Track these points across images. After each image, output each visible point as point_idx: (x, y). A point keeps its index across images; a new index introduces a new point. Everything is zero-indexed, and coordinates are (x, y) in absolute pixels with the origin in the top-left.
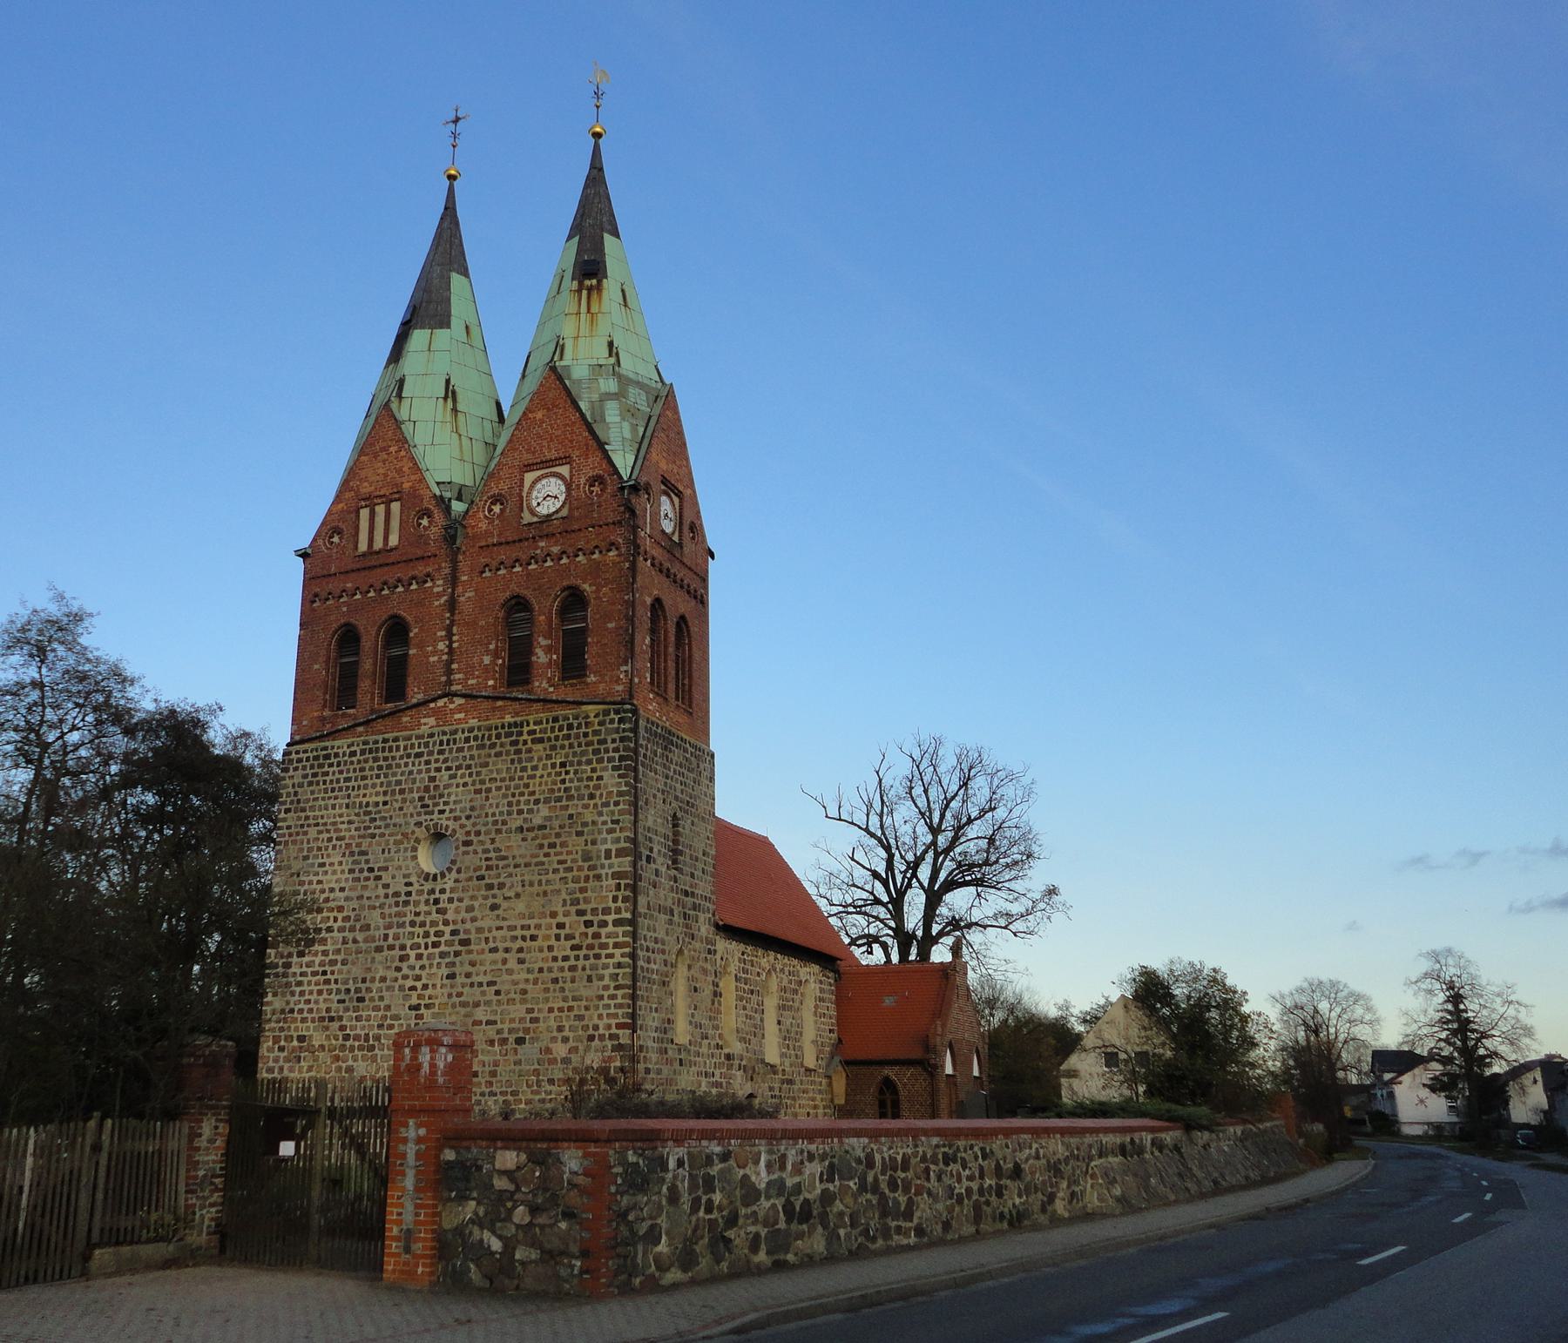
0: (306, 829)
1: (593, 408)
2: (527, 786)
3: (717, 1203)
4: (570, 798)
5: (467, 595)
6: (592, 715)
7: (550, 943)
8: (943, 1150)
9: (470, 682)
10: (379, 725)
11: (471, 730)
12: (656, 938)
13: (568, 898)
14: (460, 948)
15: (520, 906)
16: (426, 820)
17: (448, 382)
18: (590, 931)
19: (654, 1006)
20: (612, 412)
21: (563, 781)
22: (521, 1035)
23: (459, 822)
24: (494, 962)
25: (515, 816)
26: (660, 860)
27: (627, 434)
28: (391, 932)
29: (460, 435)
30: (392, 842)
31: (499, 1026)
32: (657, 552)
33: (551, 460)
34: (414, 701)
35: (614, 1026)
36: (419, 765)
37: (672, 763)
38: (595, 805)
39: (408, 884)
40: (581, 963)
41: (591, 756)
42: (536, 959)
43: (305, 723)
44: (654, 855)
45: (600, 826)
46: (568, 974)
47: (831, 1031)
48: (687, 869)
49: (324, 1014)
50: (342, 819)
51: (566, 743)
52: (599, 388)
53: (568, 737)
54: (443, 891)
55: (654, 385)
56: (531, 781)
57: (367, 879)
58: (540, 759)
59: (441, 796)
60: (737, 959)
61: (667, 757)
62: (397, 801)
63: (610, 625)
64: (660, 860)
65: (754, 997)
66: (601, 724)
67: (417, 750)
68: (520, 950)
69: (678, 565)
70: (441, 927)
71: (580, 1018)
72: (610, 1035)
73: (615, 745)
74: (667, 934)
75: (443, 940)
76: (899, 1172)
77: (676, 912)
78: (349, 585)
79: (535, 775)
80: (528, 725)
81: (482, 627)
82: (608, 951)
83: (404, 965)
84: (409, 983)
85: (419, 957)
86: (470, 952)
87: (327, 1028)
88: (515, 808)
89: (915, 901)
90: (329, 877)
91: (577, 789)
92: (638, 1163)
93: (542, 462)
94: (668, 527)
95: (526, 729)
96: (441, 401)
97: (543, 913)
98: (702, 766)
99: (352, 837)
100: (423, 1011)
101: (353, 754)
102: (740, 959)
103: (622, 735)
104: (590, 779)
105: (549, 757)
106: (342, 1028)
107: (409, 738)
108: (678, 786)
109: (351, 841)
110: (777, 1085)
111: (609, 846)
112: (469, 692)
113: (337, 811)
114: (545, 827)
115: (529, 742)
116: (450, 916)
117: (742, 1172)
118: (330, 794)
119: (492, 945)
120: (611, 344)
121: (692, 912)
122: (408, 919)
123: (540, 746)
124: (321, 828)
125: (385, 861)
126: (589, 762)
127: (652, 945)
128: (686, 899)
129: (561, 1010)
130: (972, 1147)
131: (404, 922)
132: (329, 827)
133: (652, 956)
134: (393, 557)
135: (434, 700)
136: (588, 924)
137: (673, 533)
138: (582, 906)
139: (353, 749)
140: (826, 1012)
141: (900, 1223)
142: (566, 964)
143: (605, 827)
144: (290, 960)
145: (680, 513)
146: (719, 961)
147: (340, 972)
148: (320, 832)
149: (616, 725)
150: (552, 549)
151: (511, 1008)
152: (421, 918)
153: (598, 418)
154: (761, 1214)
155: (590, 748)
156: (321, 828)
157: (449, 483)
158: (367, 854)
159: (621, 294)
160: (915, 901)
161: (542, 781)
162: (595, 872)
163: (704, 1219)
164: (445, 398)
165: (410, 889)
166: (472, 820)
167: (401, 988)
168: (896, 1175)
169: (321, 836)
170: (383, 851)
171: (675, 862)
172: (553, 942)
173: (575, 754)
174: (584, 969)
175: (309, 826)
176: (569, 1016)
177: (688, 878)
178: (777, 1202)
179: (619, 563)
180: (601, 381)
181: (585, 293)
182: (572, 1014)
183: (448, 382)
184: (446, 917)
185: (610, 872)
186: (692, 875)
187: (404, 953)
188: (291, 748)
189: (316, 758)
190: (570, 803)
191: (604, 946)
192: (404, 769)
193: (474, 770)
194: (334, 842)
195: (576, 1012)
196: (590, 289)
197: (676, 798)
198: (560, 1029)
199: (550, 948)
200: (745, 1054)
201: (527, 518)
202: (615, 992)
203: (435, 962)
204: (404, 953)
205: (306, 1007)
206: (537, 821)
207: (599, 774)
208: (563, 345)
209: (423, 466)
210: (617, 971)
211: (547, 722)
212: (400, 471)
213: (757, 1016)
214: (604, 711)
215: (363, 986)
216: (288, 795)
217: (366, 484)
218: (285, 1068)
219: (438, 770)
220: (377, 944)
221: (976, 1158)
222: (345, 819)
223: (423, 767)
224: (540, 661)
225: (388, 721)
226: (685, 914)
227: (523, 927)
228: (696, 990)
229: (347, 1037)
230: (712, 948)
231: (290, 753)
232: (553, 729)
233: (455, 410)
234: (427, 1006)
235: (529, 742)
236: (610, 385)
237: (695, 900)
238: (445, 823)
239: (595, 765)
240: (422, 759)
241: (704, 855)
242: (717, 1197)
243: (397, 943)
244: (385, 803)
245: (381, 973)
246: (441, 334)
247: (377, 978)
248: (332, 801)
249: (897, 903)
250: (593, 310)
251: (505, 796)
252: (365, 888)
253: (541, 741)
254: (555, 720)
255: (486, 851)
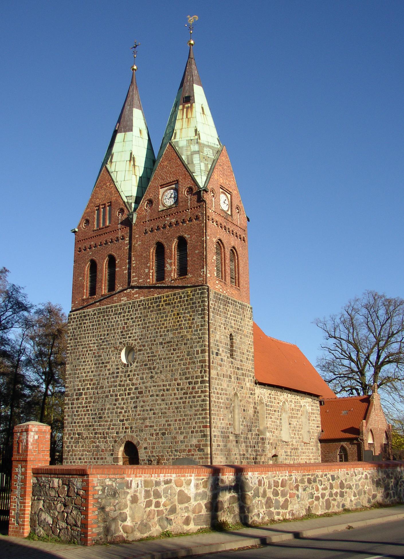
0: (78, 347)
1: (188, 158)
2: (163, 324)
3: (163, 503)
4: (181, 328)
5: (138, 243)
6: (189, 292)
7: (175, 392)
8: (307, 477)
9: (140, 281)
10: (104, 302)
11: (141, 301)
12: (222, 388)
13: (181, 372)
14: (138, 395)
15: (163, 377)
16: (124, 341)
17: (131, 154)
18: (191, 386)
19: (222, 418)
20: (196, 159)
21: (178, 321)
22: (164, 431)
23: (137, 342)
24: (153, 400)
25: (159, 337)
26: (223, 354)
27: (203, 168)
28: (111, 389)
29: (136, 176)
30: (110, 351)
31: (155, 428)
32: (217, 218)
33: (171, 182)
34: (118, 290)
35: (202, 427)
36: (121, 318)
37: (229, 311)
38: (192, 331)
39: (118, 369)
40: (187, 400)
41: (190, 310)
42: (170, 399)
43: (77, 302)
44: (220, 352)
45: (194, 340)
46: (182, 405)
47: (317, 427)
48: (237, 358)
49: (87, 424)
50: (91, 342)
51: (179, 304)
52: (191, 149)
53: (180, 302)
54: (131, 371)
55: (216, 146)
56: (165, 322)
57: (101, 367)
58: (169, 312)
59: (129, 330)
60: (266, 397)
61: (226, 309)
62: (112, 333)
63: (196, 252)
64: (223, 354)
65: (276, 413)
66: (193, 295)
67: (119, 311)
68: (163, 395)
69: (230, 224)
70: (131, 387)
71: (187, 423)
72: (200, 430)
73: (200, 304)
74: (228, 386)
75: (132, 392)
76: (280, 487)
77: (232, 377)
78: (92, 243)
79: (167, 319)
80: (163, 298)
81: (145, 256)
82: (198, 395)
83: (117, 403)
84: (119, 410)
85: (123, 399)
86: (142, 397)
87: (89, 430)
88: (159, 334)
89: (369, 373)
90: (87, 367)
91: (184, 324)
92: (112, 485)
93: (167, 184)
94: (225, 207)
95: (162, 300)
96: (128, 162)
97: (123, 371)
98: (245, 313)
99: (95, 350)
100: (125, 422)
101: (95, 314)
102: (268, 397)
103: (202, 300)
104: (189, 320)
105: (172, 311)
106: (94, 430)
107: (117, 306)
108: (233, 321)
109: (95, 351)
110: (289, 451)
111: (198, 349)
112: (140, 285)
113: (90, 339)
114: (171, 342)
115: (164, 305)
116: (134, 381)
117: (179, 489)
118: (86, 332)
119: (151, 393)
120: (196, 131)
121: (241, 377)
122: (117, 384)
123: (169, 307)
124: (83, 346)
125: (108, 359)
126: (189, 312)
127: (220, 391)
128: (238, 371)
129: (180, 420)
130: (326, 475)
131: (117, 385)
132: (87, 346)
133: (220, 396)
134: (109, 229)
135: (126, 290)
136: (190, 383)
137: (228, 210)
138: (188, 376)
139: (95, 312)
140: (315, 419)
141: (279, 510)
142: (181, 401)
143: (196, 340)
144: (73, 401)
145: (231, 201)
146: (256, 398)
147: (93, 406)
148: (83, 348)
149: (200, 295)
150: (172, 220)
151: (160, 420)
152: (123, 383)
153: (190, 162)
154: (191, 508)
155: (189, 306)
156: (83, 346)
157: (131, 196)
158: (101, 357)
159: (201, 109)
160: (369, 373)
161: (170, 322)
162: (192, 360)
163: (155, 511)
164: (130, 161)
165: (118, 371)
166: (142, 340)
167: (116, 413)
168: (277, 489)
169: (84, 350)
170: (108, 354)
171: (232, 355)
172: (176, 391)
173: (183, 309)
174: (189, 403)
175: (79, 345)
176: (183, 423)
177: (239, 362)
178: (201, 502)
179: (199, 224)
180: (192, 146)
181: (185, 110)
182: (184, 422)
183: (131, 154)
184: (133, 382)
185: (198, 360)
186: (241, 361)
187: (116, 398)
188: (71, 313)
189: (81, 317)
190: (181, 331)
191: (197, 392)
192: (114, 320)
193: (142, 319)
194: (89, 352)
195: (186, 421)
196: (188, 108)
197: (232, 327)
198: (180, 429)
199: (175, 394)
200: (271, 437)
201: (161, 207)
202: (202, 412)
203: (129, 401)
204: (116, 398)
205: (80, 421)
206: (168, 339)
207: (193, 317)
208: (176, 132)
209: (120, 190)
210: (202, 403)
211: (171, 296)
212: (111, 193)
213: (278, 421)
214: (194, 289)
215: (102, 412)
216: (71, 333)
217: (98, 200)
218: (74, 446)
219: (128, 319)
220: (106, 394)
221: (329, 480)
222: (93, 342)
223: (122, 318)
224: (168, 269)
225: (108, 300)
226: (238, 378)
227: (163, 386)
228: (244, 410)
229: (96, 433)
230: (253, 392)
231: (71, 316)
232: (173, 299)
233: (134, 165)
234: (127, 420)
235: (164, 305)
236: (195, 148)
237: (243, 372)
238: (131, 342)
239: (191, 314)
240: (122, 315)
241: (247, 352)
242: (163, 500)
243: (114, 394)
244: (108, 335)
245: (108, 406)
246: (128, 134)
247: (107, 408)
248: (87, 335)
249: (362, 373)
250: (188, 117)
251: (155, 329)
252: (101, 371)
253: (169, 304)
254: (175, 295)
255: (148, 353)
